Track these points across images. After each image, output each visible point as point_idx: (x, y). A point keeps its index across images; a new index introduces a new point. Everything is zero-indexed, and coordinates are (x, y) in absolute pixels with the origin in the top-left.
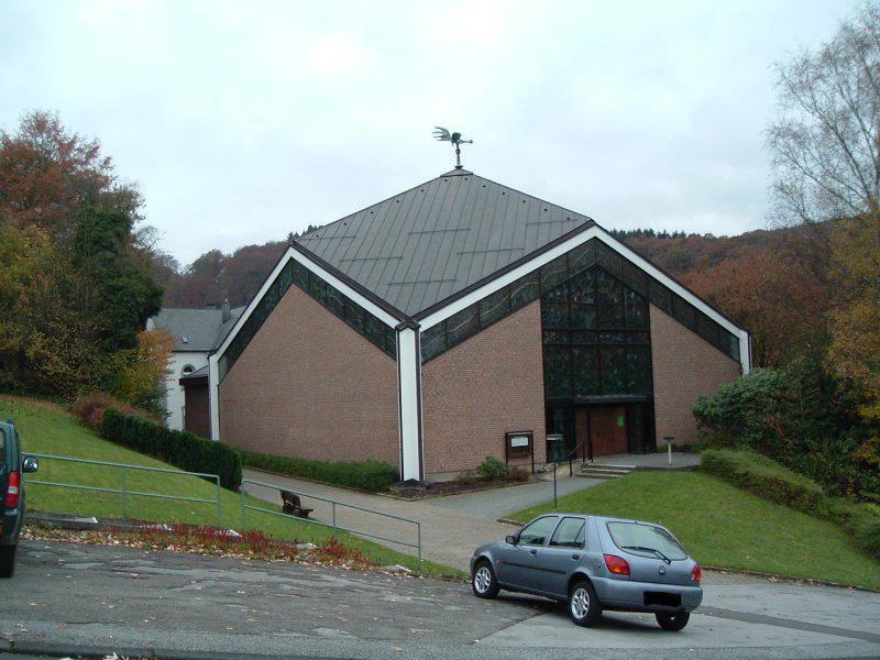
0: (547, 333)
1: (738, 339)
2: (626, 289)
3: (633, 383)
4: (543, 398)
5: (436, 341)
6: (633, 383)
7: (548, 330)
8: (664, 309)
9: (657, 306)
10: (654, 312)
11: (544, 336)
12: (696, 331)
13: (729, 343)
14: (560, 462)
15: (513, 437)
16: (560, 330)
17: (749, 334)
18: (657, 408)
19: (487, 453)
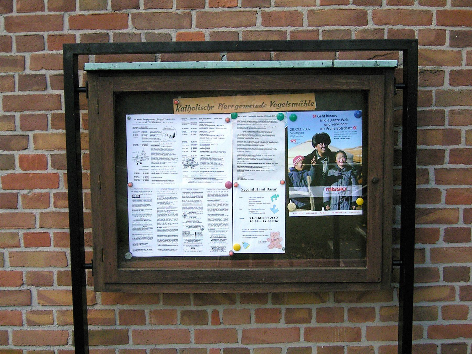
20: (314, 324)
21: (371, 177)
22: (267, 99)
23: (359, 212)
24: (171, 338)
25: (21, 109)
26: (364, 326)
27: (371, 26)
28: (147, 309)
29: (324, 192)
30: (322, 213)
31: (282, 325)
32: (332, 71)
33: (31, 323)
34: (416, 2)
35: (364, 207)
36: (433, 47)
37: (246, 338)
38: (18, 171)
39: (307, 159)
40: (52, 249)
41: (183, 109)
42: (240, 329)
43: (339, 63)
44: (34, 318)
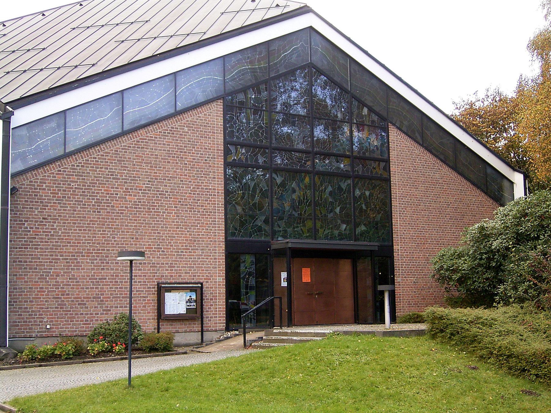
0: (232, 148)
1: (512, 183)
2: (355, 103)
3: (363, 228)
4: (222, 238)
5: (226, 338)
6: (363, 228)
7: (235, 144)
8: (409, 134)
9: (399, 129)
10: (395, 135)
11: (227, 152)
12: (455, 168)
13: (501, 189)
14: (430, 339)
15: (169, 290)
16: (255, 147)
17: (526, 177)
18: (397, 263)
19: (527, 402)
20: (188, 326)
21: (197, 302)
22: (177, 291)
23: (195, 307)
24: (168, 328)
25: (54, 278)
26: (195, 326)
27: (195, 280)
28: (164, 324)
29: (191, 304)
30: (191, 307)
31: (183, 326)
32: (193, 287)
33: (147, 326)
34: (370, 317)
35: (196, 306)
36: (414, 328)
37: (179, 328)
38: (146, 302)
39: (189, 299)
40: (151, 314)
41: (172, 292)
42: (177, 326)
43: (194, 286)
44: (148, 326)
